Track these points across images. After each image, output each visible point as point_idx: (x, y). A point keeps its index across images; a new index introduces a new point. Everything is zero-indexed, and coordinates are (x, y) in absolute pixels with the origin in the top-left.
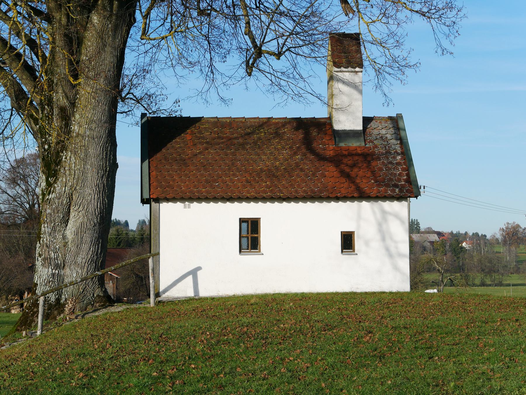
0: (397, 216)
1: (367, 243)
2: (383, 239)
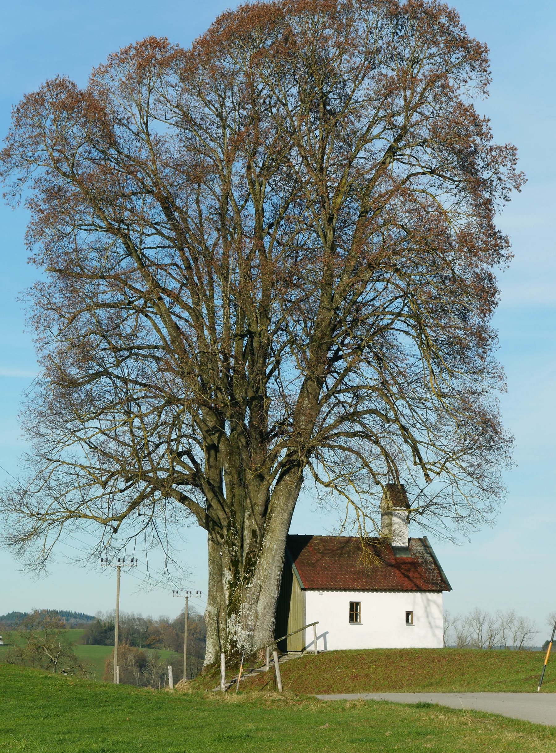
0: (435, 603)
1: (418, 619)
2: (428, 617)
